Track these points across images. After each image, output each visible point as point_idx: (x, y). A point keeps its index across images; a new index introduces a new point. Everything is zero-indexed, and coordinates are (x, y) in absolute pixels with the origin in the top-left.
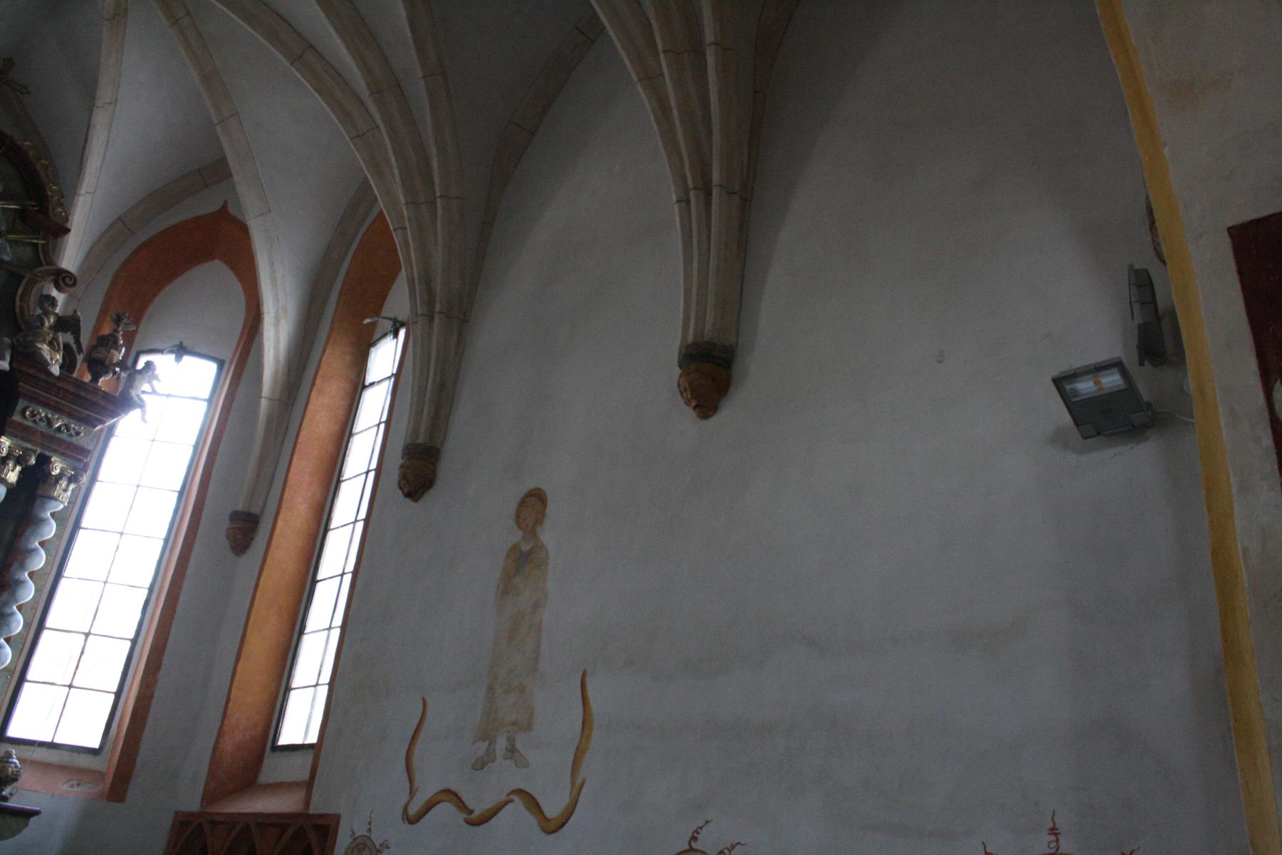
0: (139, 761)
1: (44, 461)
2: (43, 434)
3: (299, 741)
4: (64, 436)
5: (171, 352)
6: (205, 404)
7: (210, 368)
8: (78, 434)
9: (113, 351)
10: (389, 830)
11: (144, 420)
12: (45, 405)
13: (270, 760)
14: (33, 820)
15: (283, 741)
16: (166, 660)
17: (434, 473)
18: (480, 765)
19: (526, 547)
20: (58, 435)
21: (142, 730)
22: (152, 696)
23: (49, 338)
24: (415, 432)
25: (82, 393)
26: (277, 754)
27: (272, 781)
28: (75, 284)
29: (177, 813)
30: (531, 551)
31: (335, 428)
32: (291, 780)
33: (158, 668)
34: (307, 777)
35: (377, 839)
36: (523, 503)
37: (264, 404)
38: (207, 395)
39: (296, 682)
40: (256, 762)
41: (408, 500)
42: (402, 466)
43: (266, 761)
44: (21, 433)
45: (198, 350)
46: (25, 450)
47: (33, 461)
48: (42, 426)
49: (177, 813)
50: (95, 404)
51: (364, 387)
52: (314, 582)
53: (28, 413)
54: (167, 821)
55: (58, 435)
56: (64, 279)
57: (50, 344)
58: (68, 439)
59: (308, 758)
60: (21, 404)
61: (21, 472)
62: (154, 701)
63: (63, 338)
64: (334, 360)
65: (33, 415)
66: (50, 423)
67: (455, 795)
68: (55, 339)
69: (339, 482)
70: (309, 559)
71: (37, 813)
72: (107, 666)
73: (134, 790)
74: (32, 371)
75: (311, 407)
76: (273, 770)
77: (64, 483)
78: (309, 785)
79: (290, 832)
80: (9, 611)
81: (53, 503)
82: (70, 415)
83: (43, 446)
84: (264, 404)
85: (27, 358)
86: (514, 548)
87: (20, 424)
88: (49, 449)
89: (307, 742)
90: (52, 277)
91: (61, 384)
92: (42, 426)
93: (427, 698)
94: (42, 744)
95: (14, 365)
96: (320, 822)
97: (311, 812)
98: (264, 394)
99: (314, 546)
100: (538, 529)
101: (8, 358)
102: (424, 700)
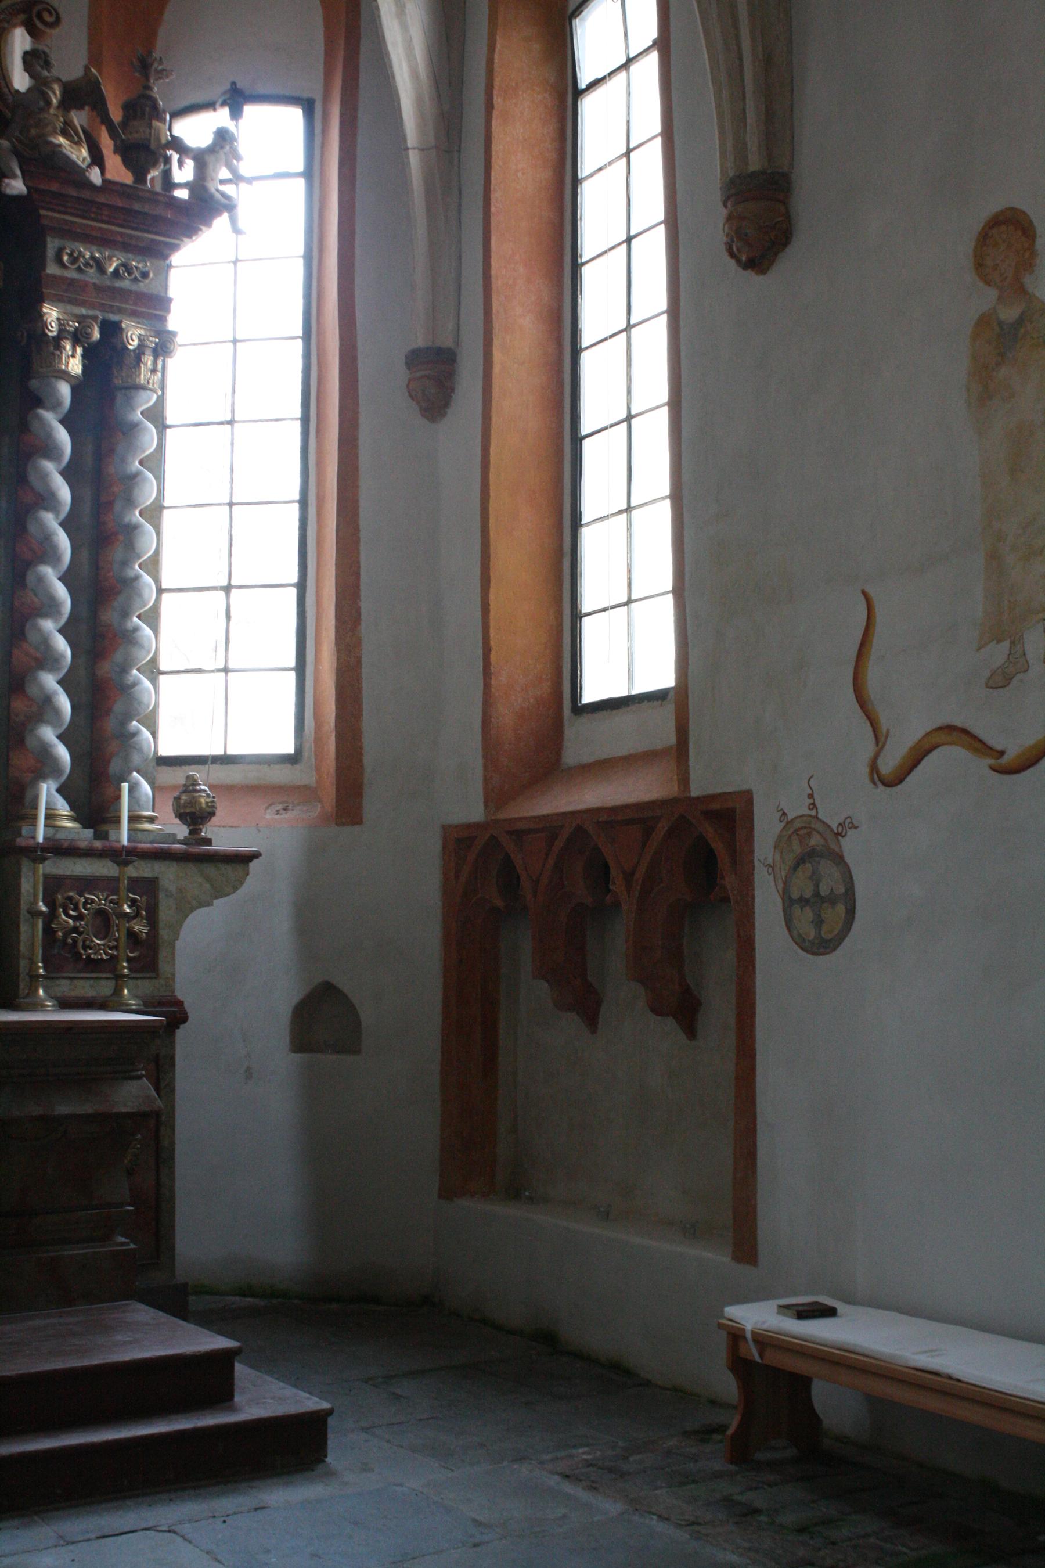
0: (368, 760)
1: (112, 330)
2: (98, 288)
3: (618, 690)
4: (126, 284)
5: (224, 104)
6: (301, 182)
7: (295, 115)
8: (145, 275)
9: (156, 123)
10: (847, 798)
11: (237, 231)
12: (88, 239)
13: (574, 731)
14: (254, 865)
15: (589, 696)
16: (365, 605)
17: (788, 217)
18: (1001, 680)
19: (1009, 314)
20: (119, 284)
21: (358, 715)
22: (359, 662)
23: (59, 125)
24: (741, 151)
25: (137, 206)
26: (585, 719)
27: (587, 759)
28: (58, 20)
29: (446, 829)
30: (1020, 321)
31: (545, 175)
32: (623, 752)
33: (357, 620)
34: (672, 740)
35: (830, 815)
36: (984, 238)
37: (414, 158)
38: (299, 166)
39: (588, 602)
40: (551, 736)
41: (749, 274)
42: (729, 218)
43: (569, 732)
44: (70, 293)
45: (261, 90)
46: (81, 319)
47: (96, 335)
48: (91, 275)
49: (446, 829)
50: (157, 219)
51: (578, 93)
52: (578, 441)
53: (65, 257)
54: (434, 844)
55: (119, 284)
56: (39, 16)
57: (65, 133)
58: (134, 287)
59: (669, 710)
60: (52, 245)
61: (84, 356)
62: (365, 671)
63: (79, 118)
64: (516, 56)
65: (74, 260)
66: (101, 269)
67: (965, 731)
68: (68, 123)
69: (576, 267)
70: (559, 405)
71: (255, 855)
72: (270, 628)
73: (370, 806)
74: (55, 187)
75: (497, 147)
76: (581, 743)
77: (148, 359)
78: (681, 749)
79: (662, 828)
80: (131, 574)
81: (143, 394)
82: (126, 247)
83: (103, 307)
84: (414, 158)
85: (44, 164)
86: (984, 321)
87: (62, 279)
88: (111, 309)
89: (635, 691)
90: (22, 17)
91: (102, 199)
92: (91, 275)
93: (868, 589)
94: (216, 760)
95: (30, 184)
96: (716, 806)
97: (694, 793)
98: (410, 144)
99: (561, 384)
100: (1027, 280)
101: (18, 172)
102: (864, 593)
